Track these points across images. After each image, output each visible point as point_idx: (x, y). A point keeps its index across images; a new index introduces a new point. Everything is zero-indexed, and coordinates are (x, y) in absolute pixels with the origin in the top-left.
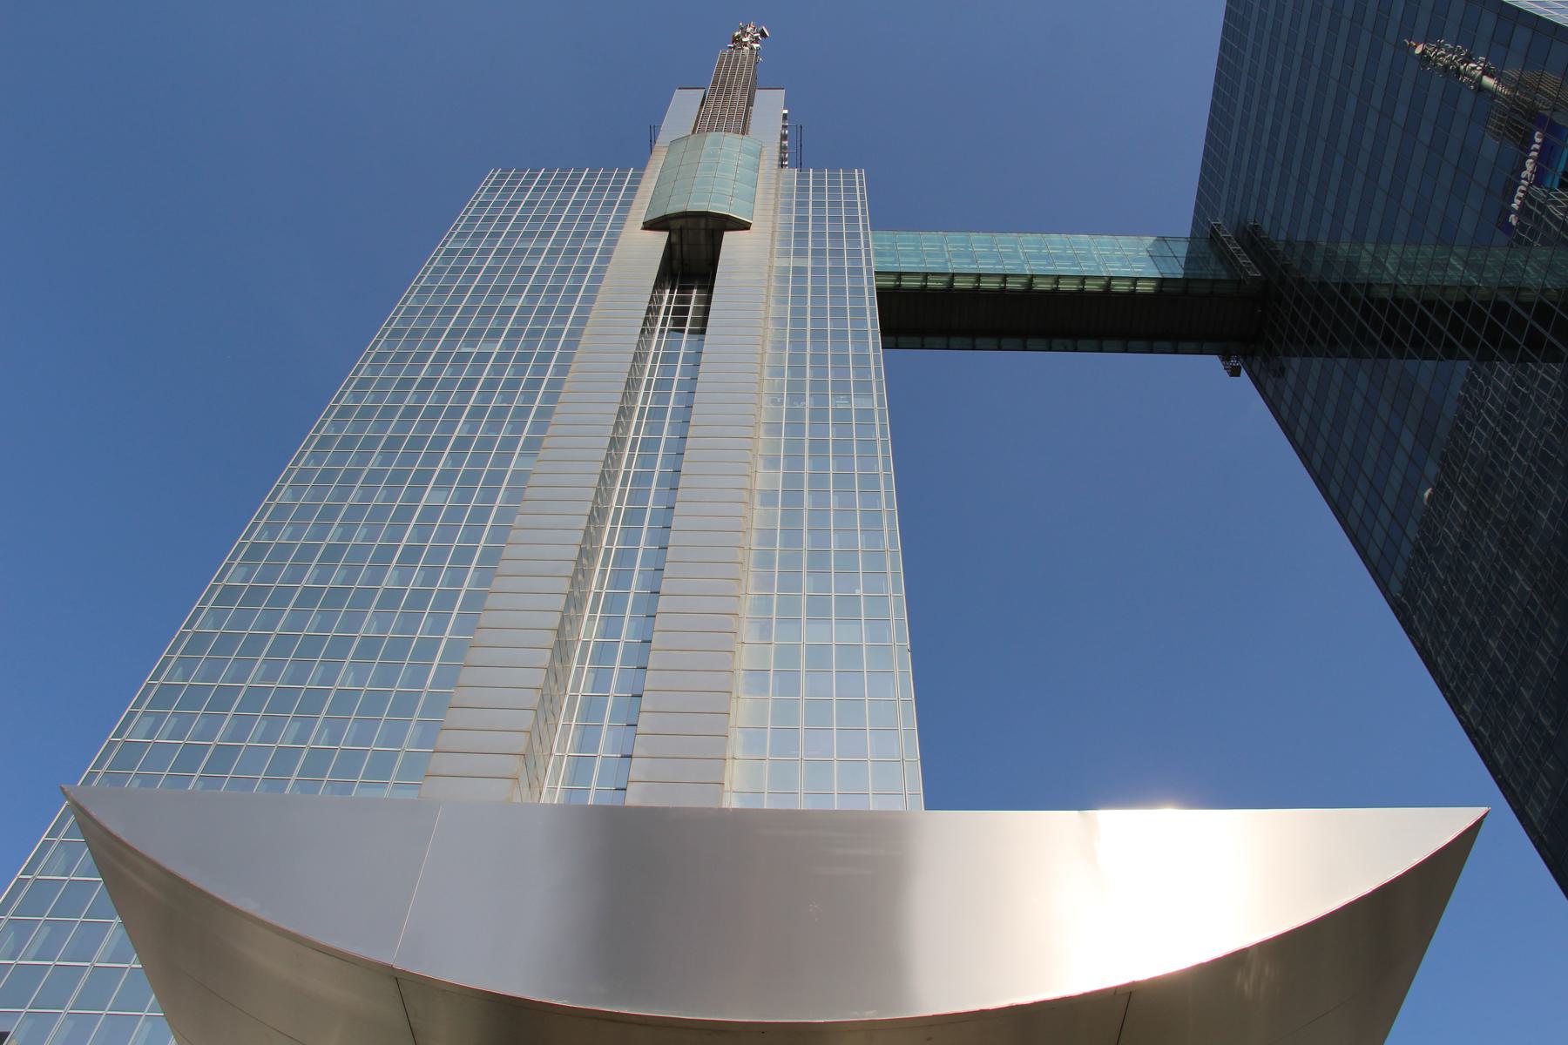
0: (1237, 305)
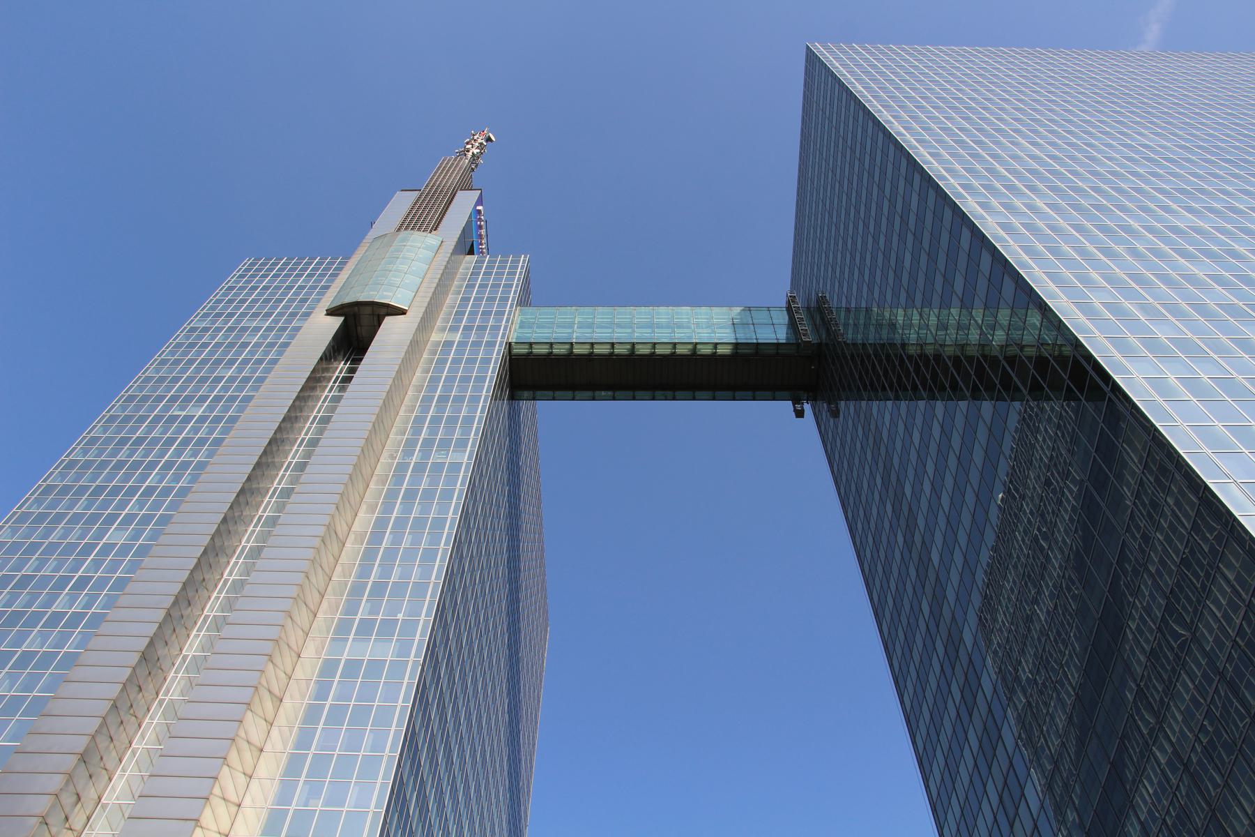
0: (803, 368)
